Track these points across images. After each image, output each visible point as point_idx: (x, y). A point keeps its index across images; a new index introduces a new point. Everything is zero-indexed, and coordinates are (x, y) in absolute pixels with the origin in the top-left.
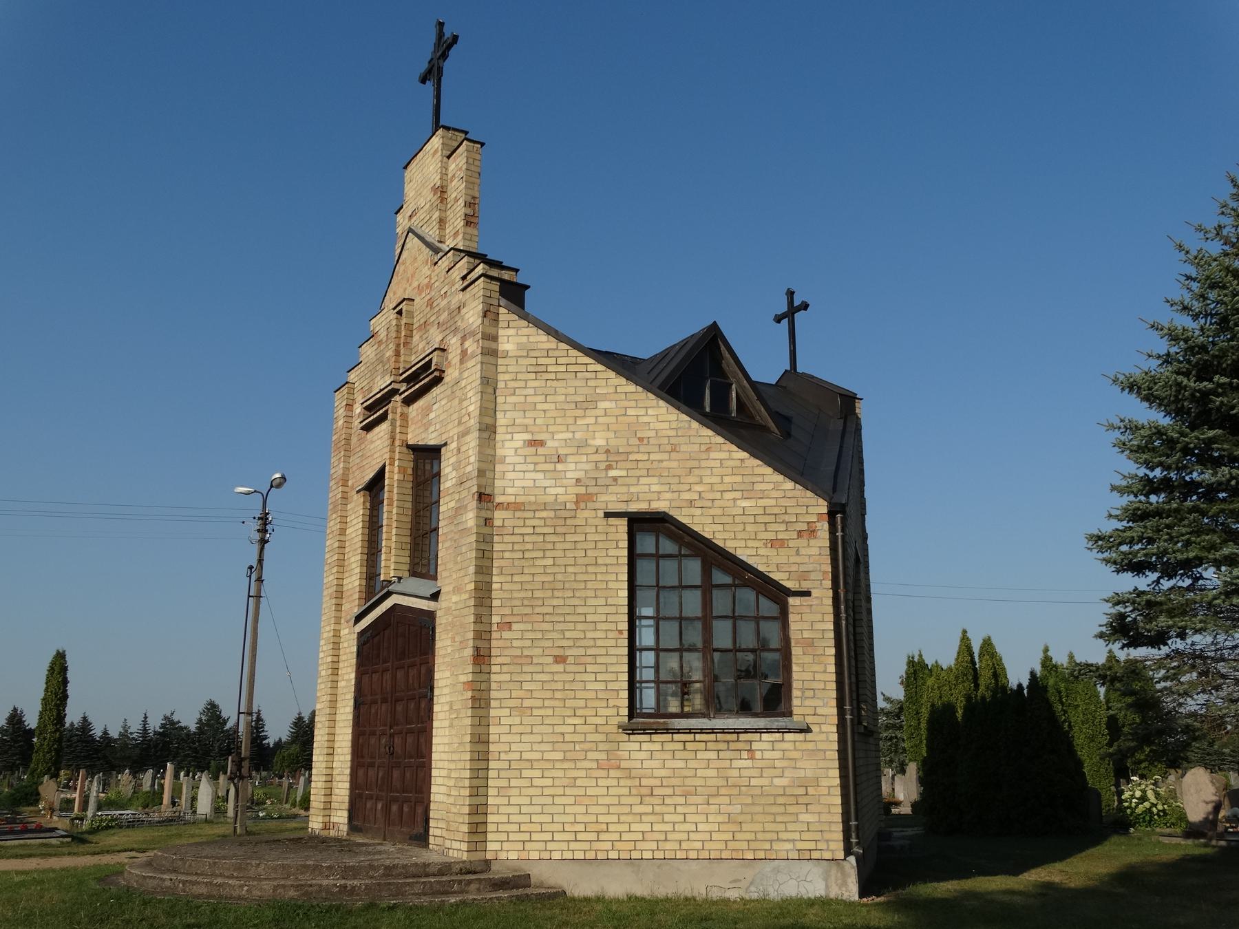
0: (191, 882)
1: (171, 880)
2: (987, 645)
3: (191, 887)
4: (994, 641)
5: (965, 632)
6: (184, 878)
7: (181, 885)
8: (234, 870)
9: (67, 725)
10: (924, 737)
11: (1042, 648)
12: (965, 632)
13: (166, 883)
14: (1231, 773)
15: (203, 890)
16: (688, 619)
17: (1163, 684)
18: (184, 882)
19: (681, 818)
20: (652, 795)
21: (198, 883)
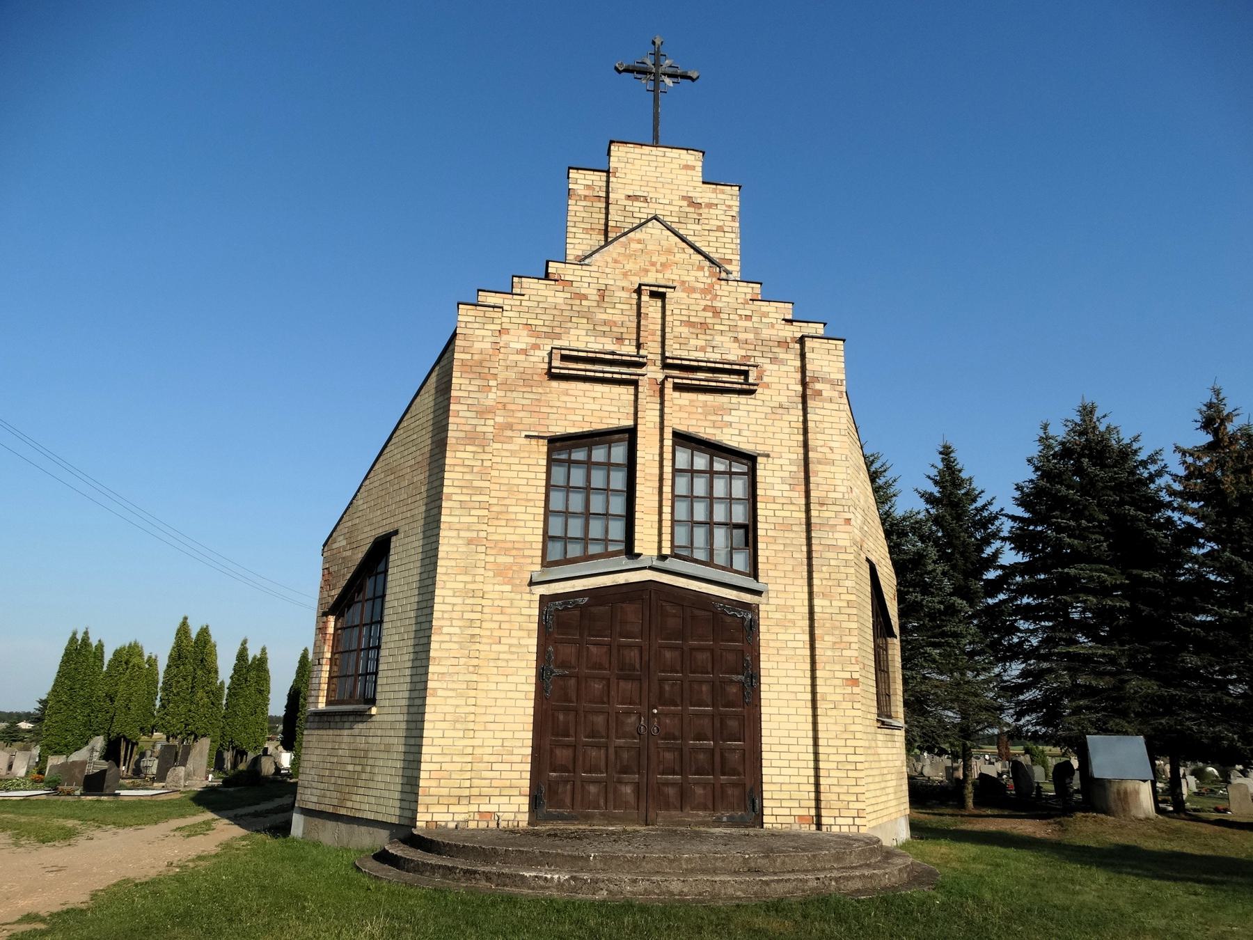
0: (844, 878)
1: (818, 879)
2: (204, 632)
3: (845, 884)
4: (211, 632)
5: (186, 618)
6: (835, 874)
7: (833, 883)
8: (834, 862)
9: (250, 659)
10: (95, 798)
11: (242, 639)
12: (186, 618)
13: (810, 884)
14: (670, 788)
15: (858, 885)
16: (734, 499)
17: (1079, 605)
18: (837, 880)
19: (842, 797)
20: (838, 762)
21: (853, 878)
